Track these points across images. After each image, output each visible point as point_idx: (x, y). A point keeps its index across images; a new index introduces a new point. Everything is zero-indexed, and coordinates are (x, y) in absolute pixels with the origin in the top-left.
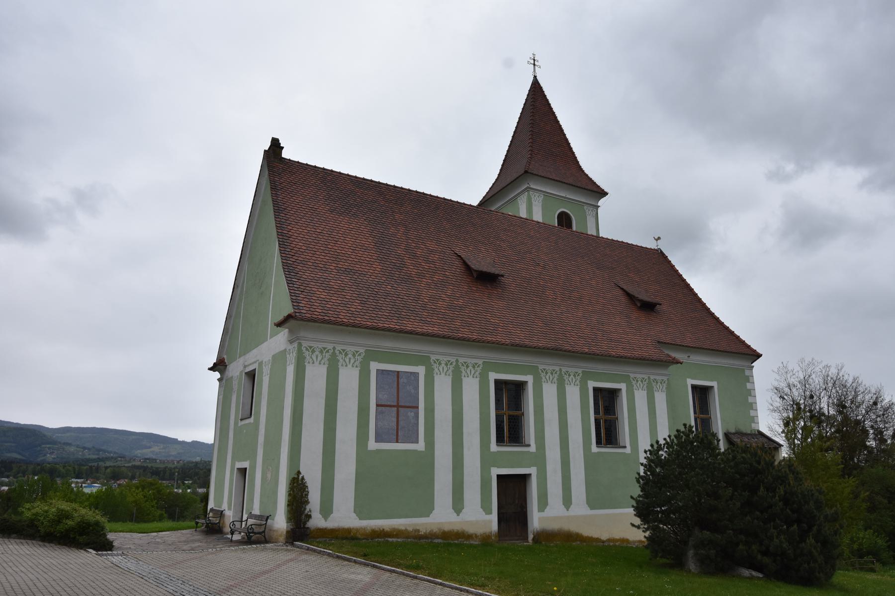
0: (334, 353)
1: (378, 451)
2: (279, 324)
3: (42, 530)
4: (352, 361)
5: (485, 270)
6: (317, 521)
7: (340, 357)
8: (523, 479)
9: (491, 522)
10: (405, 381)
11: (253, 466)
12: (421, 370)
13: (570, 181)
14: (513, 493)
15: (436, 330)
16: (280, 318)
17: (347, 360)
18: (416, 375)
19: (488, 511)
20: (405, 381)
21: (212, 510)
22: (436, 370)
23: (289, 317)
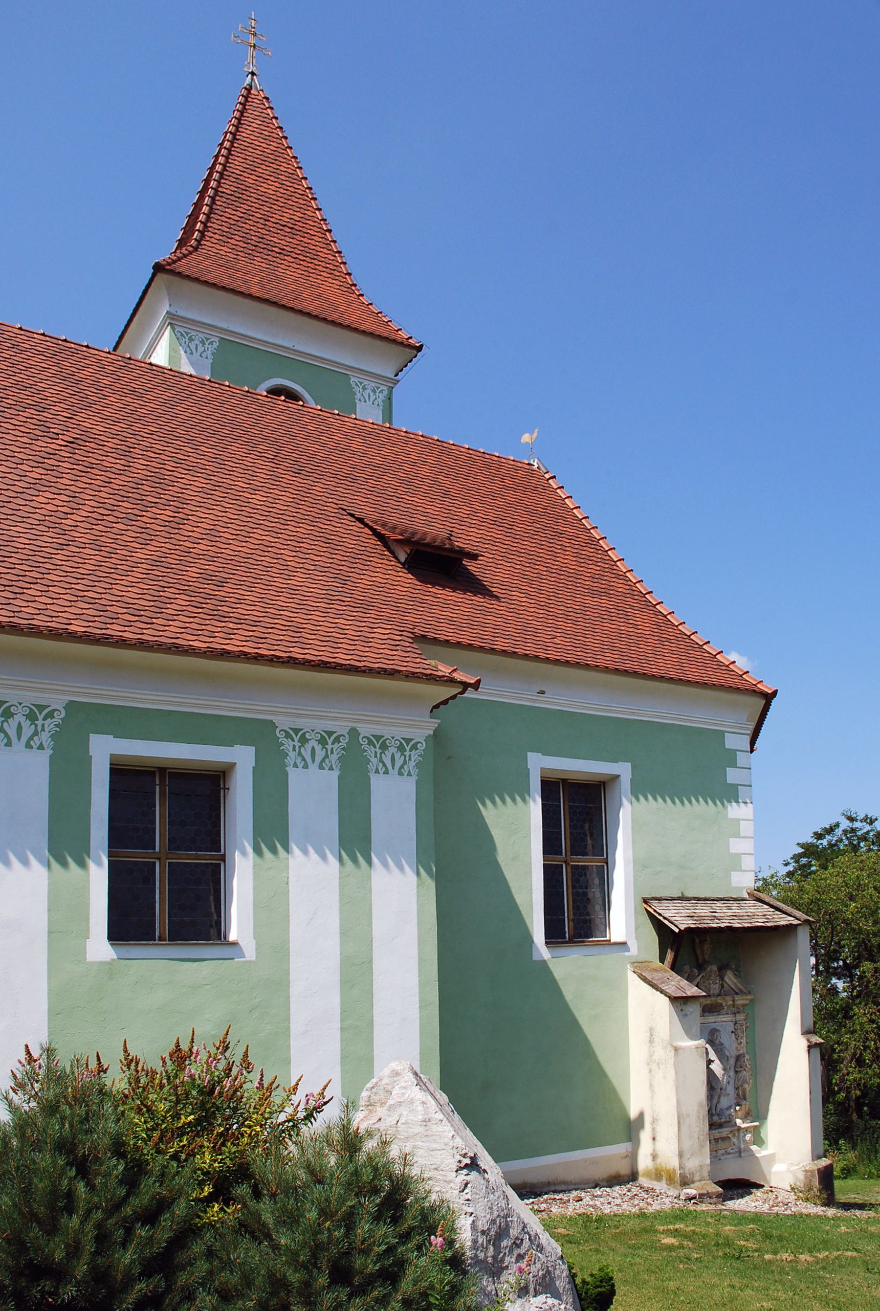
7: (370, 752)
17: (12, 732)
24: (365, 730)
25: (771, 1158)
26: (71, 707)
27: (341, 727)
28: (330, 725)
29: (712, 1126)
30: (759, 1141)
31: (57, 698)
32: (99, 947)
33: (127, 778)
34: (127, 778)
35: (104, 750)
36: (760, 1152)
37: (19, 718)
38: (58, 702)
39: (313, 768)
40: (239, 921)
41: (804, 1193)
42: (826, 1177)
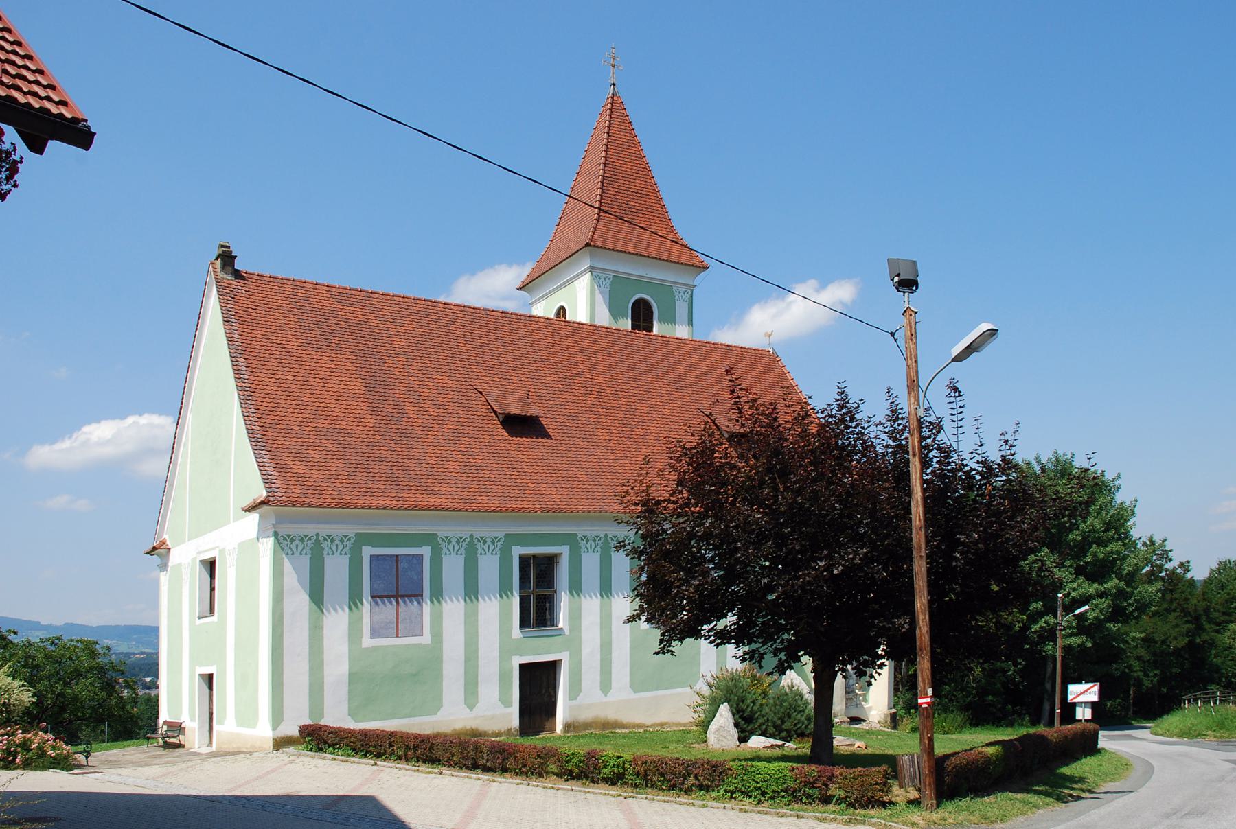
0: (317, 539)
1: (375, 649)
2: (250, 509)
3: (908, 696)
4: (340, 548)
5: (514, 411)
6: (841, 742)
7: (324, 545)
8: (551, 668)
9: (511, 717)
10: (406, 566)
11: (223, 671)
12: (425, 552)
13: (654, 252)
14: (538, 684)
15: (445, 501)
16: (248, 501)
17: (334, 548)
18: (419, 558)
19: (508, 704)
20: (406, 566)
21: (165, 723)
22: (445, 550)
23: (263, 503)
24: (477, 535)
25: (870, 708)
26: (357, 534)
27: (602, 534)
28: (496, 534)
29: (847, 693)
30: (866, 701)
31: (351, 530)
32: (516, 632)
33: (525, 561)
34: (525, 561)
35: (367, 552)
36: (866, 705)
37: (297, 542)
38: (501, 535)
39: (489, 554)
40: (562, 621)
41: (884, 724)
42: (893, 717)
